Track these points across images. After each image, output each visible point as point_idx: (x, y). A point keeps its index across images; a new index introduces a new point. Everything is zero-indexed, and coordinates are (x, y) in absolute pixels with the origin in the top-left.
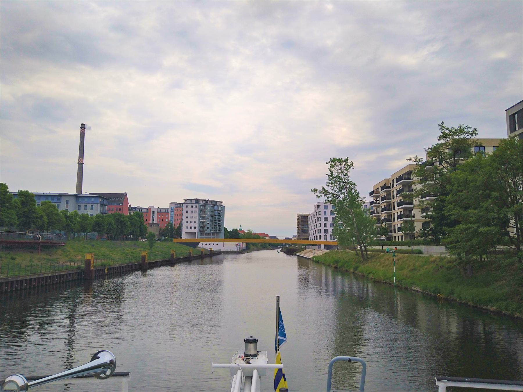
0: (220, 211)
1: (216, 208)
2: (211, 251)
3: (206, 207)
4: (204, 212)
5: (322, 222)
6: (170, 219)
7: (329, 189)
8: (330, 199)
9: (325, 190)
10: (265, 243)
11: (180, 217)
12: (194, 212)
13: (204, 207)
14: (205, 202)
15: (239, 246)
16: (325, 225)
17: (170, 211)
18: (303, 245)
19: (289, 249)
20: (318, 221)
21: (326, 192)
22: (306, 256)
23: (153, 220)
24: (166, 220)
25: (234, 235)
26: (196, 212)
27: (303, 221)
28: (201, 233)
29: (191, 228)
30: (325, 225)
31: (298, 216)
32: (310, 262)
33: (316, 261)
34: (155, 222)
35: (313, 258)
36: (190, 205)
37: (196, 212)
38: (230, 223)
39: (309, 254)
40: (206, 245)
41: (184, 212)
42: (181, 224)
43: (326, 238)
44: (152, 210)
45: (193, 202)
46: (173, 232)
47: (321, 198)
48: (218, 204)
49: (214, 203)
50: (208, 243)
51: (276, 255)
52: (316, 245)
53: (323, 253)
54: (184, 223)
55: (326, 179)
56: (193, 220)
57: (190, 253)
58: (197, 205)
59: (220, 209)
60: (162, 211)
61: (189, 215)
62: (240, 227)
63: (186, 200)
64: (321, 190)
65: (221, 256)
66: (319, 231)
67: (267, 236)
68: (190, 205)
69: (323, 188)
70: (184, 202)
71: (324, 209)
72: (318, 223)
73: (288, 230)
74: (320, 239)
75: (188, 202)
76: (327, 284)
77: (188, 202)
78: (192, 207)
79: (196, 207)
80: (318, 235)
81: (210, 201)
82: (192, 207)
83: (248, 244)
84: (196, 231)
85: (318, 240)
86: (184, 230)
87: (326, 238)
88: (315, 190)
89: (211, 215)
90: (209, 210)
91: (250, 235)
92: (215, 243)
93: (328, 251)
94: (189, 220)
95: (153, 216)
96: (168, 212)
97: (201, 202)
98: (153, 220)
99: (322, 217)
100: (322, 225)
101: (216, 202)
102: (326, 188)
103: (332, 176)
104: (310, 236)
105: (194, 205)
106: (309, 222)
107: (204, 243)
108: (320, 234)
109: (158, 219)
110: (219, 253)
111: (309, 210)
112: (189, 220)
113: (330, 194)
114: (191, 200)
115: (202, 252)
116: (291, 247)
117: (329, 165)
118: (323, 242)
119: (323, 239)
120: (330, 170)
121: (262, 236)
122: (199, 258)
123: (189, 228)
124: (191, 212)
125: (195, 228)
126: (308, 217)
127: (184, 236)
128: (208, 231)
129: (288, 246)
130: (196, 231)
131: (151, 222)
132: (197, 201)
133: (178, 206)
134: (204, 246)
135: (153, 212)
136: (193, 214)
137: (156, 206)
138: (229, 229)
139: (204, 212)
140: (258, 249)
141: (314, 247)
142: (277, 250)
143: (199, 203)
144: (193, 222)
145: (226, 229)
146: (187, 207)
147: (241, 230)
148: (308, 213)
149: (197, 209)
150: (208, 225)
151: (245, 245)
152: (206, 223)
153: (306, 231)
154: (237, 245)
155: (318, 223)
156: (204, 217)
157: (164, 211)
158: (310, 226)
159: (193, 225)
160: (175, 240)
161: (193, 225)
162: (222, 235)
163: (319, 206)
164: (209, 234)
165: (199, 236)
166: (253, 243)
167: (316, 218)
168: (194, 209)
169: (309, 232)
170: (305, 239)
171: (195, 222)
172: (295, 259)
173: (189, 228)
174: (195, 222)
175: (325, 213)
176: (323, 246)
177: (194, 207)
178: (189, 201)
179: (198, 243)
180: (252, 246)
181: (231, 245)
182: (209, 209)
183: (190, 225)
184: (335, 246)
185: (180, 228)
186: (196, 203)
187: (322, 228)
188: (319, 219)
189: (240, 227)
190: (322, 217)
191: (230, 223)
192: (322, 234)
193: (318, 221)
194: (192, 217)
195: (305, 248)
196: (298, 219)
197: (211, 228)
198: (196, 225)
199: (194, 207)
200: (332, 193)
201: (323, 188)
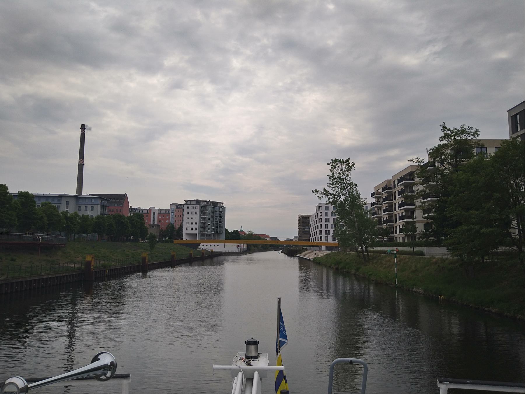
0: (221, 212)
1: (217, 209)
2: (212, 252)
3: (207, 208)
4: (205, 213)
5: (324, 223)
6: (171, 219)
7: (330, 190)
8: (331, 200)
9: (326, 191)
10: (266, 245)
11: (180, 218)
12: (194, 213)
13: (205, 208)
14: (205, 203)
15: (239, 248)
16: (326, 226)
17: (170, 212)
18: (304, 246)
19: (290, 249)
20: (319, 222)
21: (327, 193)
22: (307, 257)
23: (154, 221)
24: (167, 222)
25: (235, 236)
26: (196, 213)
27: (304, 222)
28: (202, 235)
29: (192, 229)
30: (326, 226)
31: (299, 218)
32: (311, 263)
33: (317, 262)
34: (156, 223)
35: (314, 259)
36: (190, 207)
37: (196, 213)
38: (231, 224)
39: (310, 255)
40: (206, 247)
41: (185, 213)
42: (181, 225)
43: (327, 240)
44: (152, 212)
45: (194, 203)
46: (173, 233)
47: (322, 199)
48: (219, 205)
49: (215, 204)
50: (209, 244)
51: (277, 255)
52: (317, 246)
53: (325, 254)
54: (184, 224)
55: (328, 180)
56: (194, 221)
57: (191, 254)
58: (198, 206)
59: (221, 210)
60: (162, 212)
61: (190, 216)
62: (241, 228)
63: (186, 201)
64: (323, 191)
65: (222, 258)
66: (320, 232)
67: (268, 237)
68: (190, 207)
69: (324, 189)
70: (185, 203)
71: (326, 210)
72: (319, 224)
73: (290, 232)
74: (321, 240)
75: (189, 203)
76: (328, 286)
77: (189, 203)
78: (193, 208)
79: (196, 208)
80: (319, 236)
81: (211, 202)
82: (193, 208)
83: (249, 246)
84: (197, 232)
85: (319, 241)
86: (185, 232)
87: (327, 240)
88: (316, 191)
89: (212, 216)
90: (210, 211)
91: (251, 236)
92: (216, 244)
93: (330, 252)
94: (190, 221)
95: (154, 217)
96: (169, 214)
97: (201, 203)
98: (154, 221)
99: (323, 218)
100: (324, 226)
101: (217, 203)
102: (328, 189)
103: (333, 177)
104: (311, 237)
105: (195, 206)
106: (311, 223)
107: (205, 244)
108: (321, 235)
109: (159, 220)
110: (220, 254)
111: (310, 211)
112: (190, 221)
113: (331, 195)
114: (191, 201)
115: (203, 253)
116: (293, 248)
117: (330, 166)
118: (324, 244)
119: (324, 241)
120: (332, 171)
121: (263, 237)
122: (187, 262)
123: (190, 229)
124: (192, 213)
125: (196, 229)
126: (309, 218)
127: (185, 238)
128: (209, 232)
129: (289, 247)
130: (197, 232)
131: (152, 224)
132: (198, 202)
133: (179, 207)
134: (205, 247)
135: (154, 213)
136: (194, 215)
137: (157, 207)
138: (230, 230)
139: (205, 213)
140: (259, 251)
141: (315, 248)
142: (278, 251)
143: (199, 204)
144: (194, 223)
145: (226, 230)
146: (188, 208)
147: (241, 231)
148: (309, 214)
149: (198, 210)
150: (209, 227)
151: (246, 247)
152: (206, 224)
153: (307, 233)
154: (238, 246)
155: (319, 224)
156: (205, 218)
157: (164, 212)
158: (312, 227)
159: (194, 226)
160: (175, 242)
161: (194, 226)
162: (223, 237)
163: (320, 207)
164: (209, 235)
165: (200, 238)
166: (254, 244)
167: (317, 219)
168: (194, 210)
169: (311, 233)
170: (306, 240)
171: (196, 223)
172: (296, 260)
173: (190, 229)
174: (196, 223)
175: (326, 214)
176: (324, 248)
177: (195, 208)
178: (189, 202)
179: (199, 245)
180: (252, 247)
181: (232, 247)
182: (210, 210)
183: (191, 226)
184: (336, 247)
185: (181, 229)
186: (196, 204)
187: (324, 230)
188: (320, 220)
189: (241, 228)
190: (323, 218)
191: (231, 224)
192: (324, 235)
193: (319, 222)
194: (192, 218)
195: (307, 250)
196: (299, 220)
197: (212, 230)
198: (197, 226)
199: (195, 208)
200: (333, 194)
201: (324, 189)
